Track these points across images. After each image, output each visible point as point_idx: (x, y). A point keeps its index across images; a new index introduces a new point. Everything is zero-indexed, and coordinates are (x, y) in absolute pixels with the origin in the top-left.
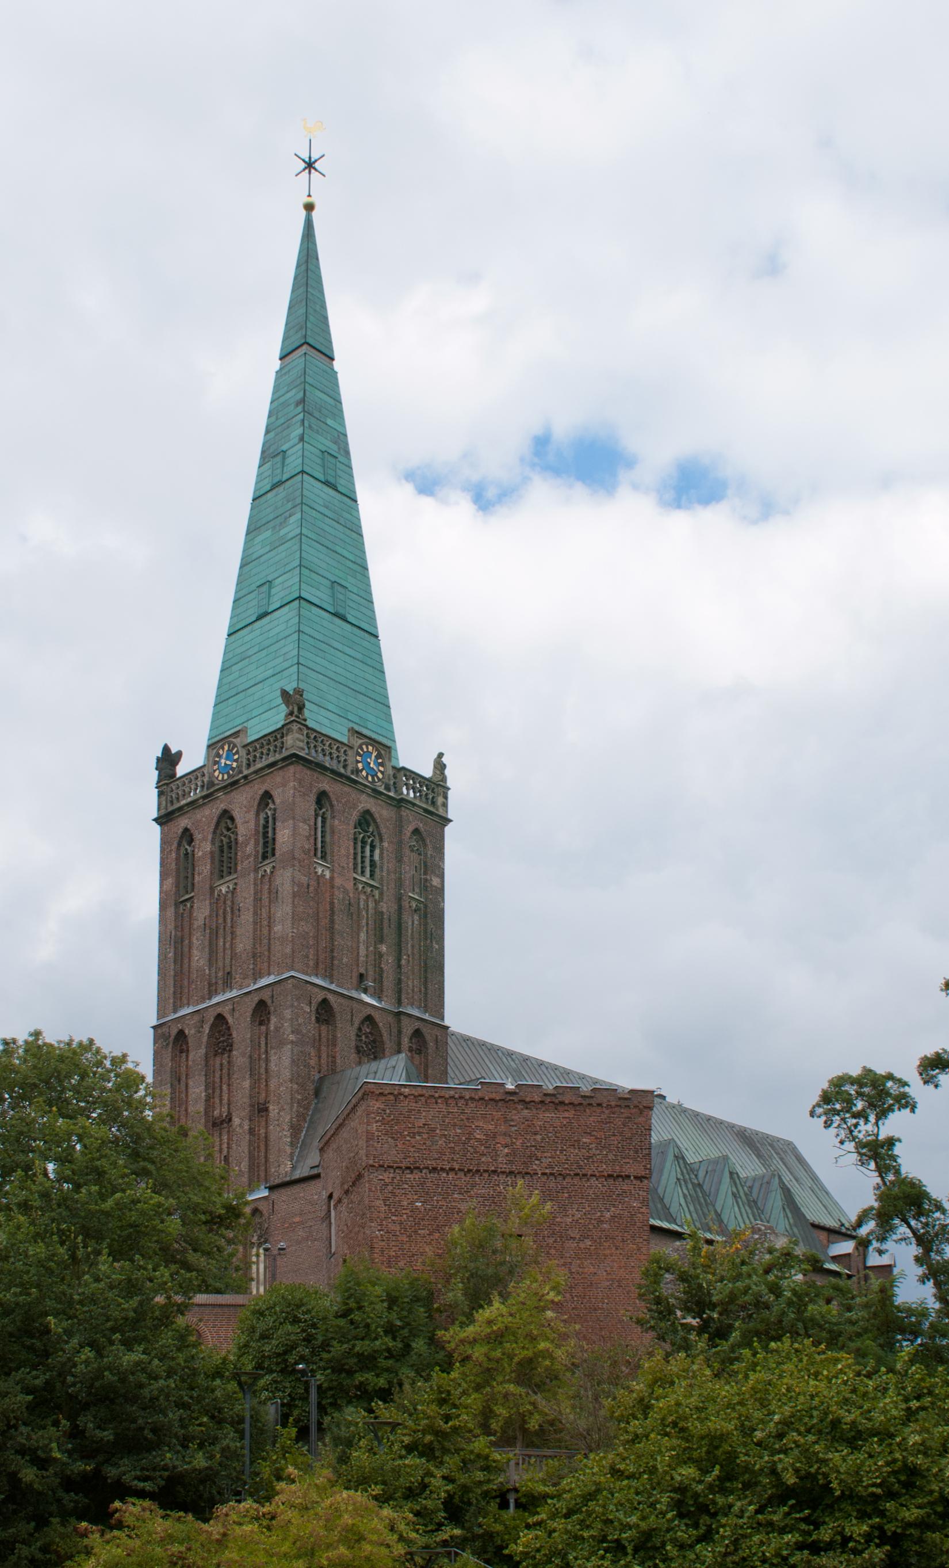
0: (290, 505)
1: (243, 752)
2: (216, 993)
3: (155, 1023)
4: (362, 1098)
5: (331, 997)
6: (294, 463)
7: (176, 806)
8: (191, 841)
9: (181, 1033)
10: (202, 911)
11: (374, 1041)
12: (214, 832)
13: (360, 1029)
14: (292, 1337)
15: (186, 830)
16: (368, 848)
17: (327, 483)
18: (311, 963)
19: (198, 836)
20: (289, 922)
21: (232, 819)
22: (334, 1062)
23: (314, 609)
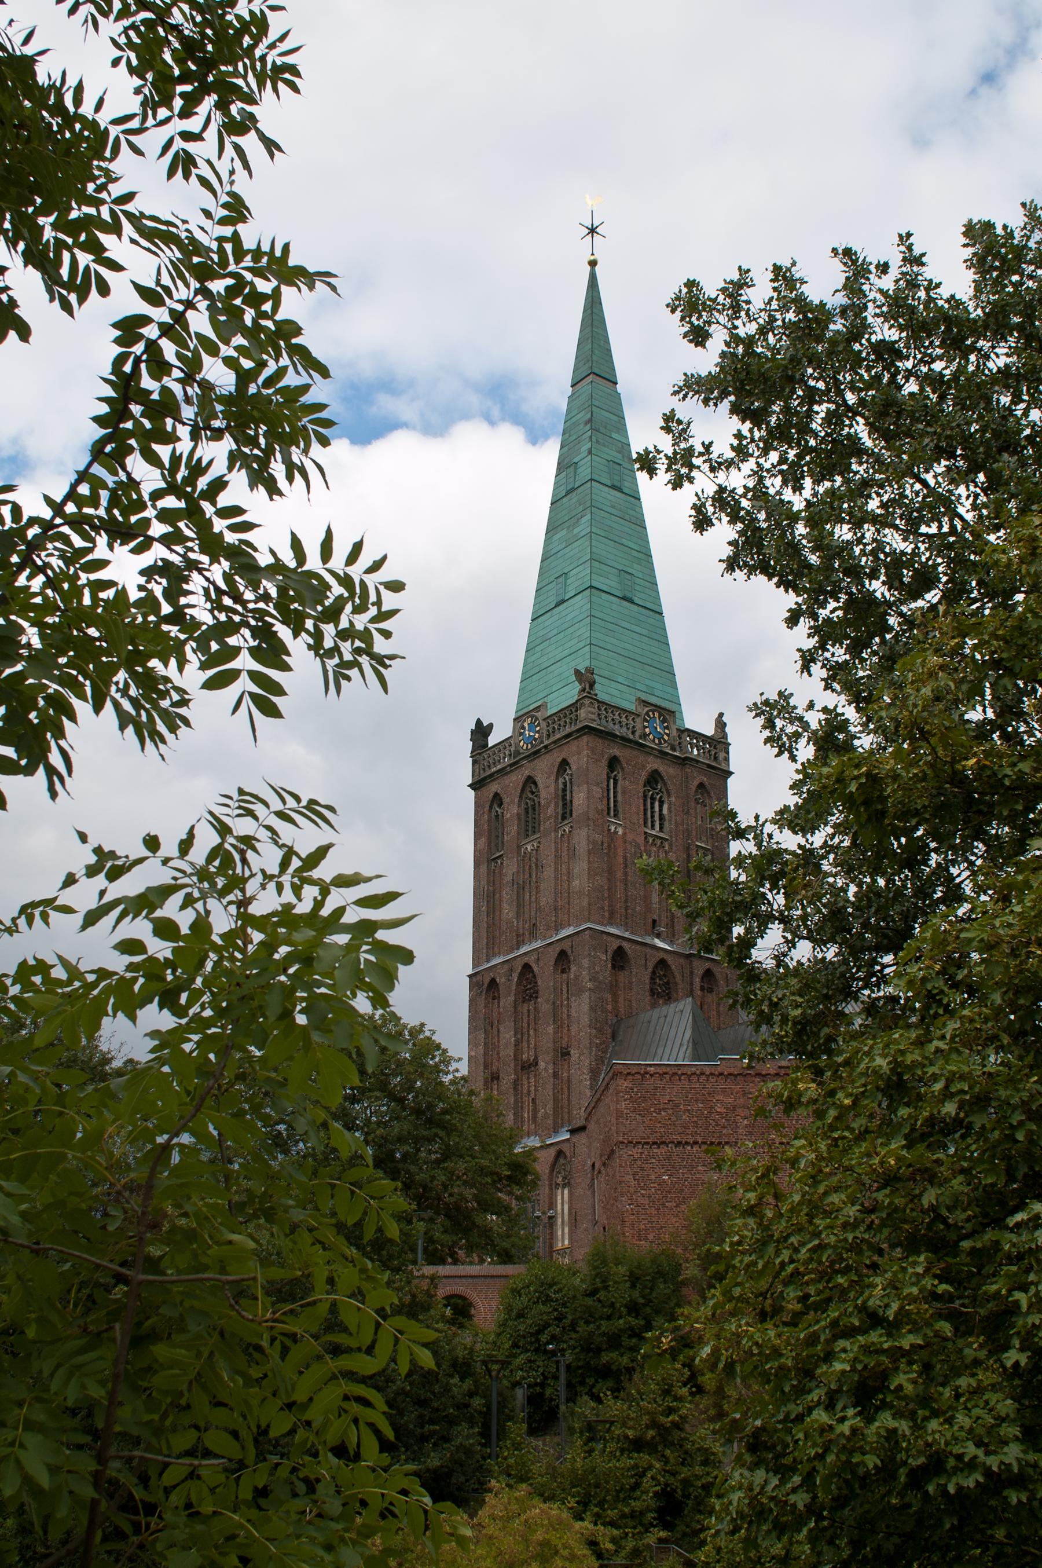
0: (581, 508)
1: (544, 724)
2: (524, 943)
3: (470, 972)
4: (612, 1078)
5: (626, 945)
6: (584, 472)
7: (488, 773)
8: (500, 805)
9: (493, 981)
10: (510, 868)
11: (668, 983)
12: (521, 797)
13: (654, 972)
14: (545, 1317)
15: (496, 794)
16: (657, 804)
17: (613, 487)
18: (607, 914)
19: (506, 800)
20: (586, 877)
21: (535, 783)
22: (630, 1006)
23: (604, 596)
